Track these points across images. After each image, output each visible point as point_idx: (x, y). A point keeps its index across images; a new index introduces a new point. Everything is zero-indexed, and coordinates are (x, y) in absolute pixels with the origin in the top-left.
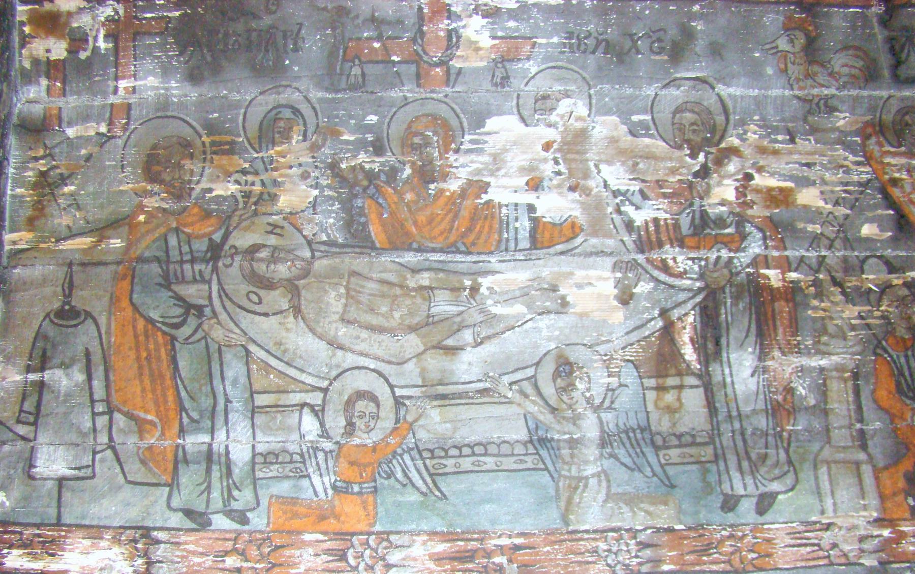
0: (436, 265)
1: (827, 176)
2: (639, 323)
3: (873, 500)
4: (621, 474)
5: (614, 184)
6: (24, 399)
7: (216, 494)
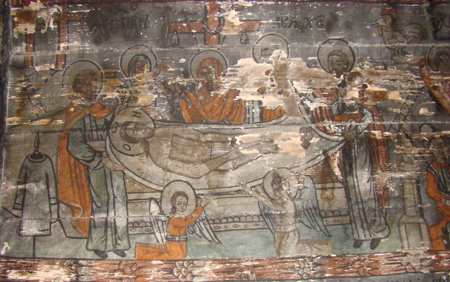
0: (214, 131)
1: (403, 85)
2: (313, 157)
3: (427, 242)
4: (305, 230)
5: (300, 90)
7: (109, 242)
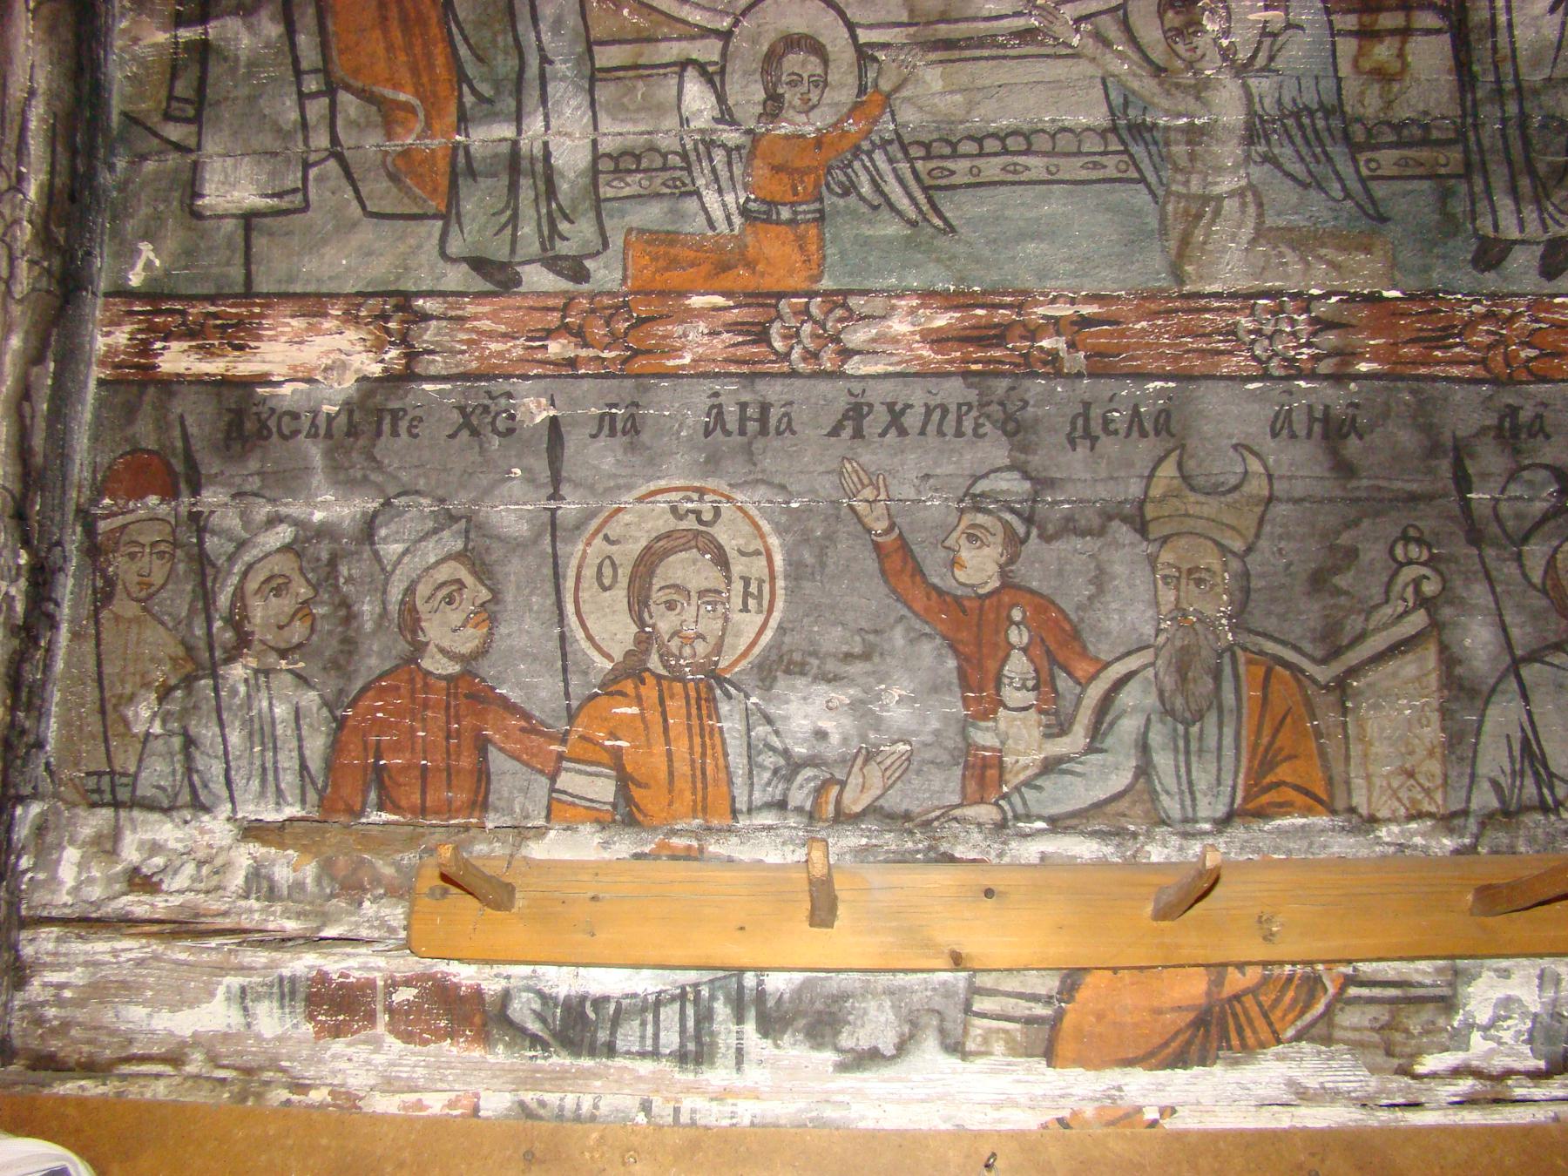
4: (1283, 193)
6: (174, 77)
7: (527, 230)
